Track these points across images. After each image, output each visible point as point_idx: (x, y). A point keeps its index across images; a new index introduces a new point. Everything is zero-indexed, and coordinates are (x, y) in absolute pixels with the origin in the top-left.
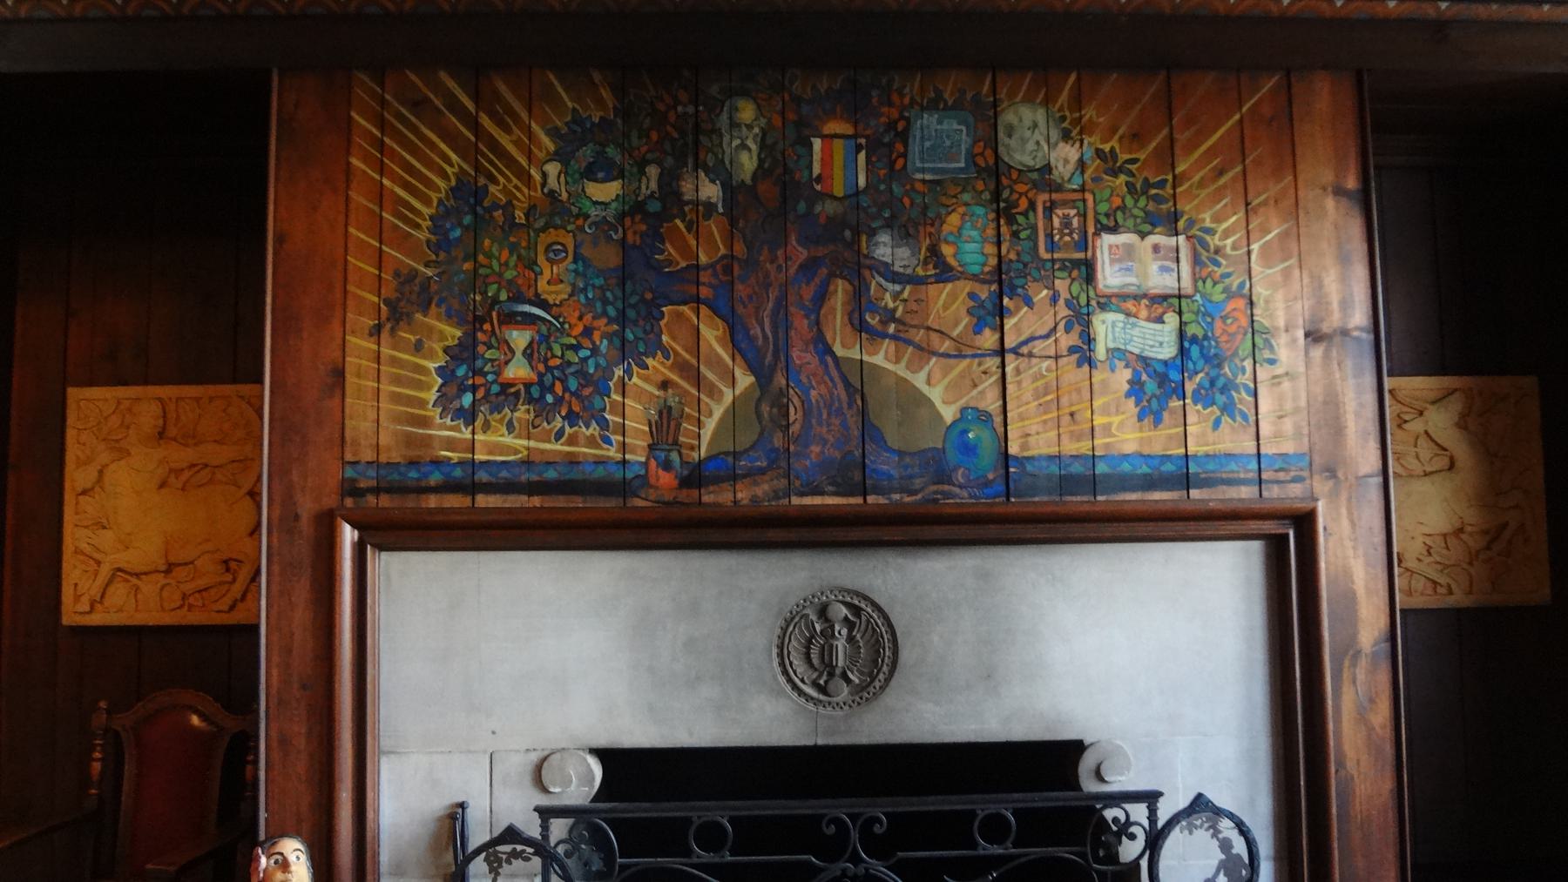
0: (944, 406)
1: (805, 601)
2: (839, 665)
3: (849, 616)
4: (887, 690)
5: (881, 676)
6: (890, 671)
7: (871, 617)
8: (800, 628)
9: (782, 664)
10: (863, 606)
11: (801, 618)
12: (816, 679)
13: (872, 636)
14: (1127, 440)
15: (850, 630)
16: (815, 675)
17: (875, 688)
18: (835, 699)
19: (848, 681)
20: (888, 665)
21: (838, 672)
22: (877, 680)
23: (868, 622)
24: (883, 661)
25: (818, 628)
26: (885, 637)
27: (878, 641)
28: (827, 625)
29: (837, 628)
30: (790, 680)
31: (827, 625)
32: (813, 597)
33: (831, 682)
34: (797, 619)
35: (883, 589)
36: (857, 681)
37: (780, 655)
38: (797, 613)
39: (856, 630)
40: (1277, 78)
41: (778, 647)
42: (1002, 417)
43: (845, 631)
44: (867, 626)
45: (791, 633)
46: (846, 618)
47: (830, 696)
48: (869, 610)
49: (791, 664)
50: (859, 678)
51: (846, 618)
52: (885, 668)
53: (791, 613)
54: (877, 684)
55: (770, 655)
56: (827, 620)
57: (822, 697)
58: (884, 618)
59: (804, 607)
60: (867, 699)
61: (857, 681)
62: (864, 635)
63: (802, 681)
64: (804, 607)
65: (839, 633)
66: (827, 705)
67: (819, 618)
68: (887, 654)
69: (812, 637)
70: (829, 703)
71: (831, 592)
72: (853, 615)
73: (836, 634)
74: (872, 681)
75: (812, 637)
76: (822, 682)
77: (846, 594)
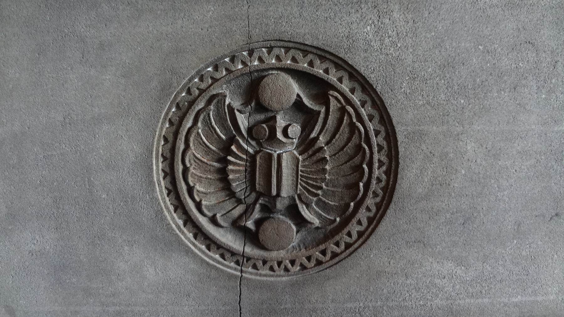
0: (169, 140)
1: (216, 68)
2: (284, 194)
3: (306, 101)
4: (373, 240)
5: (363, 215)
6: (378, 206)
7: (349, 102)
8: (208, 123)
9: (173, 191)
10: (332, 78)
11: (209, 102)
12: (240, 217)
13: (349, 140)
14: (377, 142)
15: (307, 127)
16: (239, 210)
17: (349, 234)
18: (274, 254)
19: (301, 222)
20: (375, 195)
21: (280, 205)
22: (354, 221)
23: (343, 111)
24: (367, 186)
25: (243, 121)
26: (374, 140)
27: (359, 148)
28: (261, 117)
29: (281, 122)
30: (189, 220)
31: (261, 117)
32: (233, 60)
33: (266, 224)
34: (201, 105)
35: (376, 45)
36: (317, 222)
37: (170, 174)
38: (202, 91)
39: (317, 128)
40: (254, 101)
41: (165, 158)
42: (309, 44)
43: (295, 130)
44: (340, 121)
45: (190, 129)
46: (298, 105)
47: (263, 248)
48: (345, 87)
49: (190, 190)
50: (319, 216)
51: (298, 105)
52: (370, 201)
53: (189, 92)
54: (355, 229)
55: (150, 175)
56: (261, 108)
57: (249, 250)
58: (374, 105)
59: (215, 80)
60: (335, 255)
61: (317, 222)
62: (333, 136)
63: (213, 220)
64: (215, 80)
65: (285, 132)
66: (260, 264)
67: (246, 104)
68: (376, 173)
69: (232, 140)
70: (265, 262)
71: (270, 50)
72: (315, 98)
73: (279, 135)
74: (345, 222)
75: (232, 140)
76: (250, 224)
77: (299, 56)
